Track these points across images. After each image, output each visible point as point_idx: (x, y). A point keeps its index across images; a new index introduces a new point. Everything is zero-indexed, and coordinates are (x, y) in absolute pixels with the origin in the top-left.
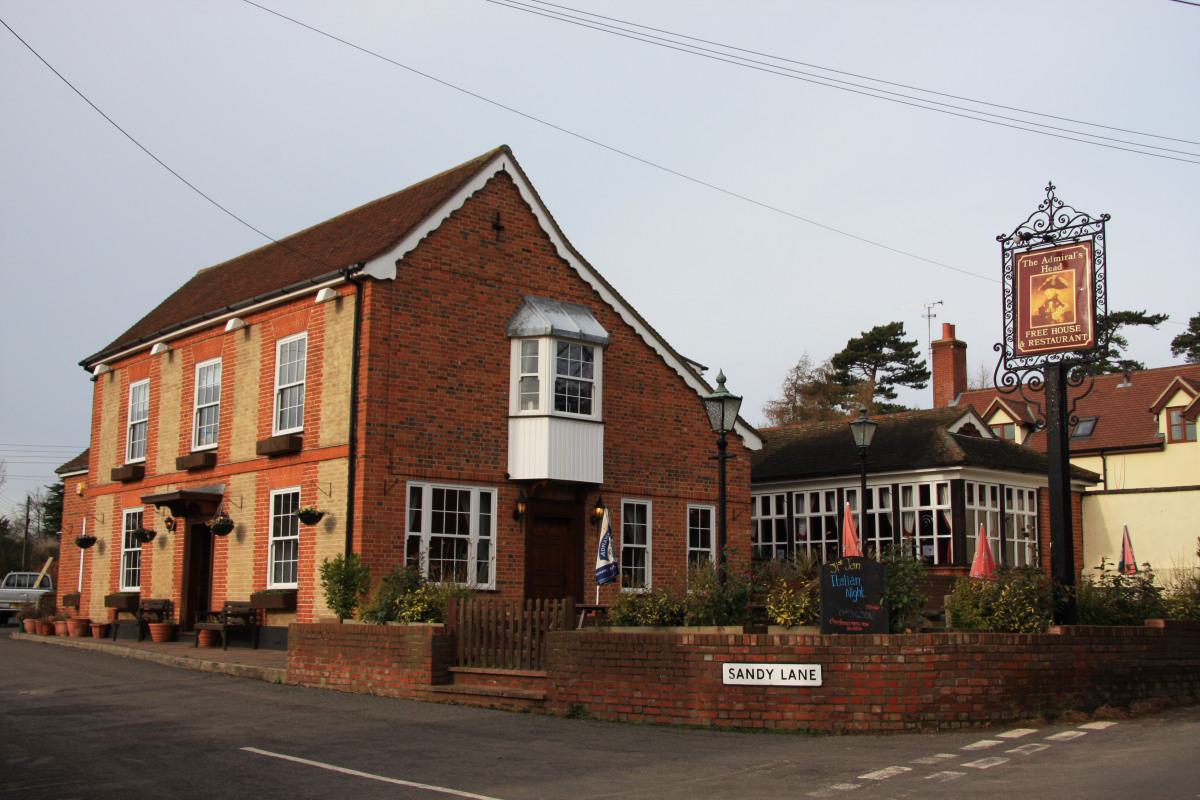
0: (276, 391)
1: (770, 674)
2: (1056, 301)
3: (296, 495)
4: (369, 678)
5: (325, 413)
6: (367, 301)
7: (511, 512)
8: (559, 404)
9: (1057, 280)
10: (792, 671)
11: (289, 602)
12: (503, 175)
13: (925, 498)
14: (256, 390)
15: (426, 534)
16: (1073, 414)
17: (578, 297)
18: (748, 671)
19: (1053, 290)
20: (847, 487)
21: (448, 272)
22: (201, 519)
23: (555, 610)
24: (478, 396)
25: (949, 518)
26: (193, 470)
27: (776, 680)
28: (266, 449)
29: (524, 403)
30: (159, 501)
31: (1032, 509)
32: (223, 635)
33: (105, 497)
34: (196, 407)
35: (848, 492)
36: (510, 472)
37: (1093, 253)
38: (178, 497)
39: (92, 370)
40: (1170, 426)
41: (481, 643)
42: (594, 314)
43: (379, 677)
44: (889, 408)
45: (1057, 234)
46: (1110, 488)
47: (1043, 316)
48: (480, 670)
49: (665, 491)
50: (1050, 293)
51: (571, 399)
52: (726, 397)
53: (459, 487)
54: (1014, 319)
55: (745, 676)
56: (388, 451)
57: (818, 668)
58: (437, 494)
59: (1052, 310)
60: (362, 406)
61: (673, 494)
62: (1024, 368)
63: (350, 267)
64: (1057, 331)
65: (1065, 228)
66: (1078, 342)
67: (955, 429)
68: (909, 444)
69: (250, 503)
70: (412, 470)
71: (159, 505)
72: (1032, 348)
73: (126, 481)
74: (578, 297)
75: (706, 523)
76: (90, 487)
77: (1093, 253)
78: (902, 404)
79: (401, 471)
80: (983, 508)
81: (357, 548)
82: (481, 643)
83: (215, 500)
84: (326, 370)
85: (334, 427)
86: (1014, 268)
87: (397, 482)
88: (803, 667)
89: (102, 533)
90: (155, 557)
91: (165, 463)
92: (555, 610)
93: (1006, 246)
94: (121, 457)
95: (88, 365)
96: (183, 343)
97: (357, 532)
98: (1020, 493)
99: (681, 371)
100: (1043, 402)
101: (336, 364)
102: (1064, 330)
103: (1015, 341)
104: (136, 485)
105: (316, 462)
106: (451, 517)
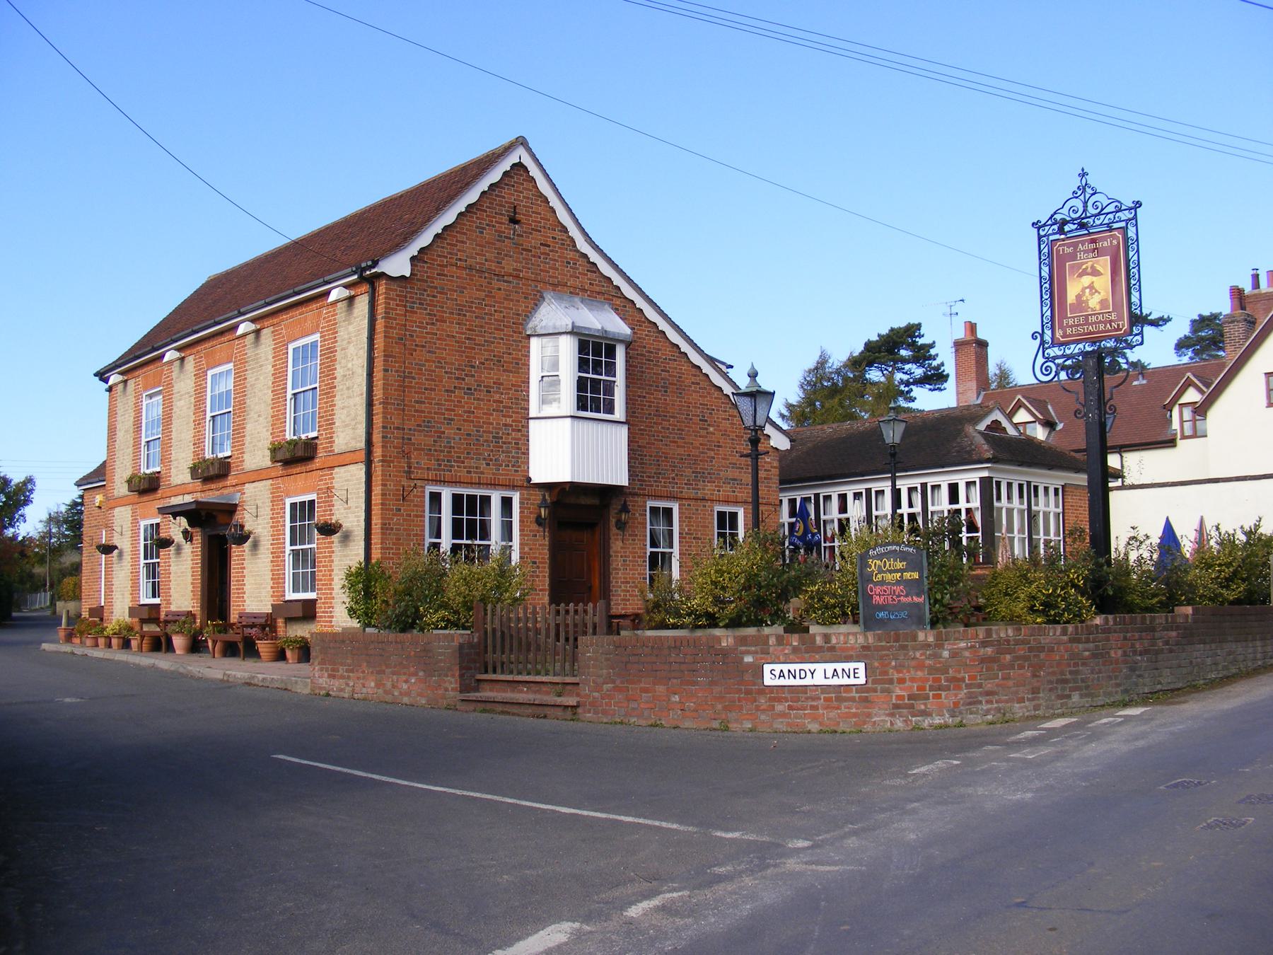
0: (289, 396)
2: (1091, 287)
3: (312, 502)
4: (394, 687)
5: (340, 417)
6: (381, 299)
7: (533, 516)
8: (582, 404)
9: (1092, 267)
11: (308, 611)
12: (519, 166)
13: (954, 498)
14: (269, 396)
15: (446, 541)
16: (1112, 402)
17: (599, 293)
20: (876, 486)
21: (465, 269)
22: (216, 529)
23: (572, 613)
24: (497, 397)
25: (978, 517)
26: (207, 480)
27: (819, 680)
28: (280, 456)
29: (544, 401)
30: (176, 512)
31: (1057, 506)
32: (241, 646)
33: (122, 509)
34: (209, 415)
35: (877, 492)
36: (531, 475)
37: (1126, 239)
38: (193, 507)
39: (106, 381)
40: (1182, 422)
41: (511, 650)
42: (616, 310)
43: (405, 686)
44: (909, 410)
45: (1091, 220)
46: (1128, 482)
48: (510, 678)
49: (692, 494)
50: (1086, 280)
51: (591, 397)
52: (758, 392)
53: (479, 492)
56: (407, 455)
57: (861, 666)
58: (457, 499)
60: (378, 408)
61: (700, 495)
62: (1063, 356)
63: (363, 265)
64: (1094, 318)
65: (1099, 214)
66: (1116, 330)
67: (982, 427)
68: (937, 442)
69: (266, 511)
70: (431, 475)
71: (175, 515)
72: (1070, 336)
73: (143, 492)
74: (599, 293)
75: (734, 525)
76: (107, 499)
77: (1126, 239)
78: (921, 408)
79: (419, 476)
81: (376, 554)
82: (511, 650)
83: (231, 509)
84: (339, 372)
85: (349, 431)
86: (1050, 254)
87: (415, 486)
88: (846, 666)
89: (123, 543)
90: (173, 569)
91: (180, 474)
92: (572, 613)
93: (1042, 233)
94: (137, 465)
95: (102, 375)
96: (194, 350)
97: (376, 539)
98: (1046, 489)
99: (706, 368)
100: (1082, 391)
101: (350, 365)
102: (1100, 317)
104: (152, 497)
105: (332, 468)
106: (472, 524)
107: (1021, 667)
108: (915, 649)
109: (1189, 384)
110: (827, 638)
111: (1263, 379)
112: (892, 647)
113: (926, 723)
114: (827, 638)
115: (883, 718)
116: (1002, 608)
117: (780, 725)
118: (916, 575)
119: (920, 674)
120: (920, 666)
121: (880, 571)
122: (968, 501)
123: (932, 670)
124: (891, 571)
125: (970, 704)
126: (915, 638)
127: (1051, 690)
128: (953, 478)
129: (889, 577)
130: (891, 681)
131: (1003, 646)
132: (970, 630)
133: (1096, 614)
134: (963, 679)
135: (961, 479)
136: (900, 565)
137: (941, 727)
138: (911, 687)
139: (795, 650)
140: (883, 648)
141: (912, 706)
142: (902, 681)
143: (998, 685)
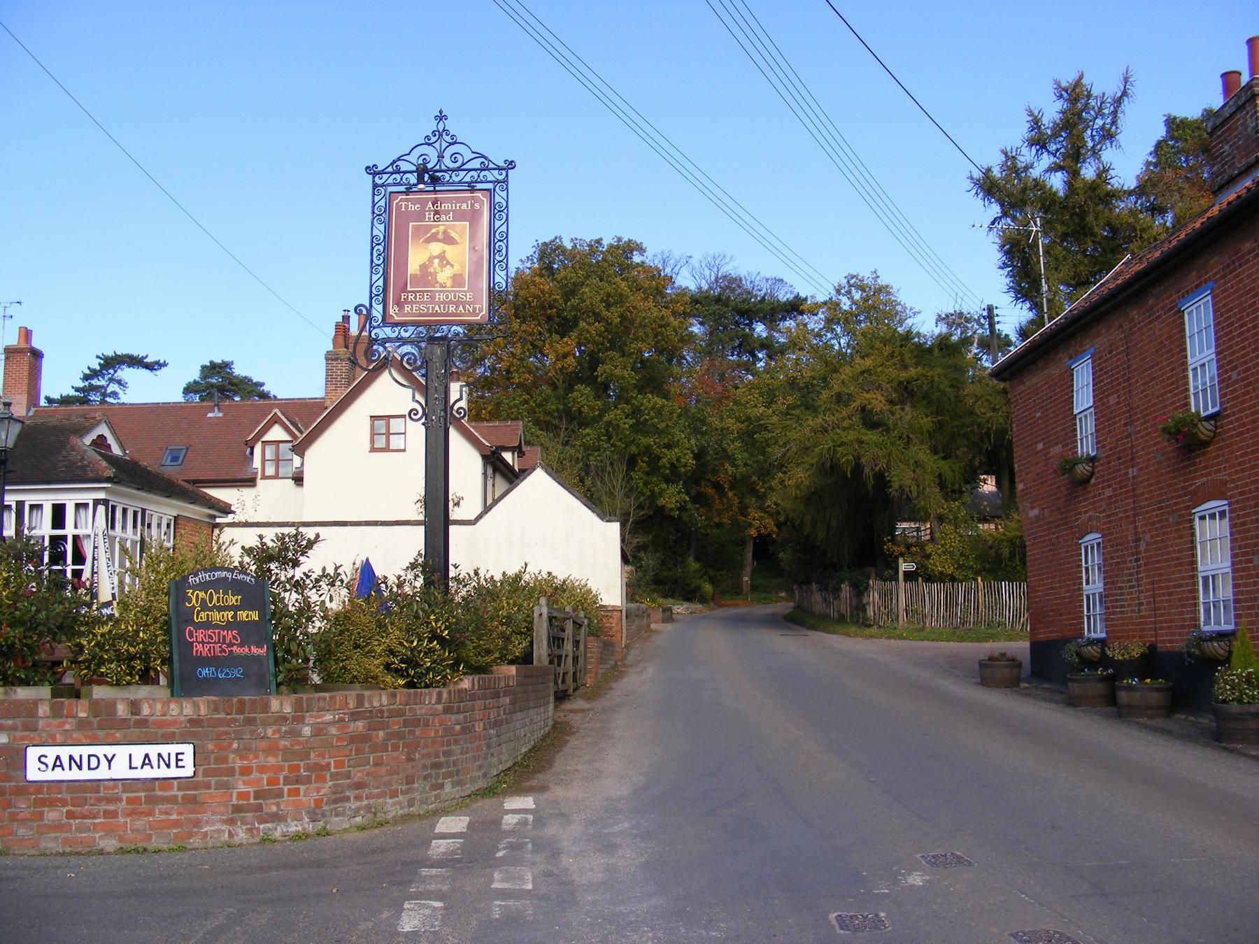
1: (110, 762)
9: (445, 232)
10: (147, 756)
18: (71, 758)
19: (441, 245)
27: (120, 770)
35: (32, 507)
40: (264, 460)
47: (426, 275)
50: (436, 248)
54: (386, 276)
55: (66, 765)
57: (188, 749)
59: (438, 269)
64: (442, 297)
65: (459, 169)
66: (470, 314)
67: (88, 440)
80: (124, 535)
88: (165, 749)
93: (378, 181)
102: (451, 296)
103: (385, 303)
107: (395, 748)
108: (266, 724)
109: (276, 420)
110: (135, 706)
111: (368, 422)
112: (234, 720)
113: (279, 831)
114: (135, 706)
115: (218, 826)
116: (352, 665)
117: (51, 843)
118: (255, 616)
119: (271, 760)
120: (272, 749)
121: (204, 607)
122: (76, 527)
123: (288, 754)
124: (220, 609)
125: (336, 801)
126: (266, 708)
127: (426, 778)
128: (60, 498)
129: (217, 616)
130: (231, 772)
131: (376, 719)
132: (339, 696)
133: (464, 674)
134: (328, 767)
135: (70, 500)
136: (233, 600)
137: (298, 837)
138: (261, 780)
139: (82, 725)
140: (221, 723)
141: (259, 808)
142: (246, 771)
143: (369, 774)
